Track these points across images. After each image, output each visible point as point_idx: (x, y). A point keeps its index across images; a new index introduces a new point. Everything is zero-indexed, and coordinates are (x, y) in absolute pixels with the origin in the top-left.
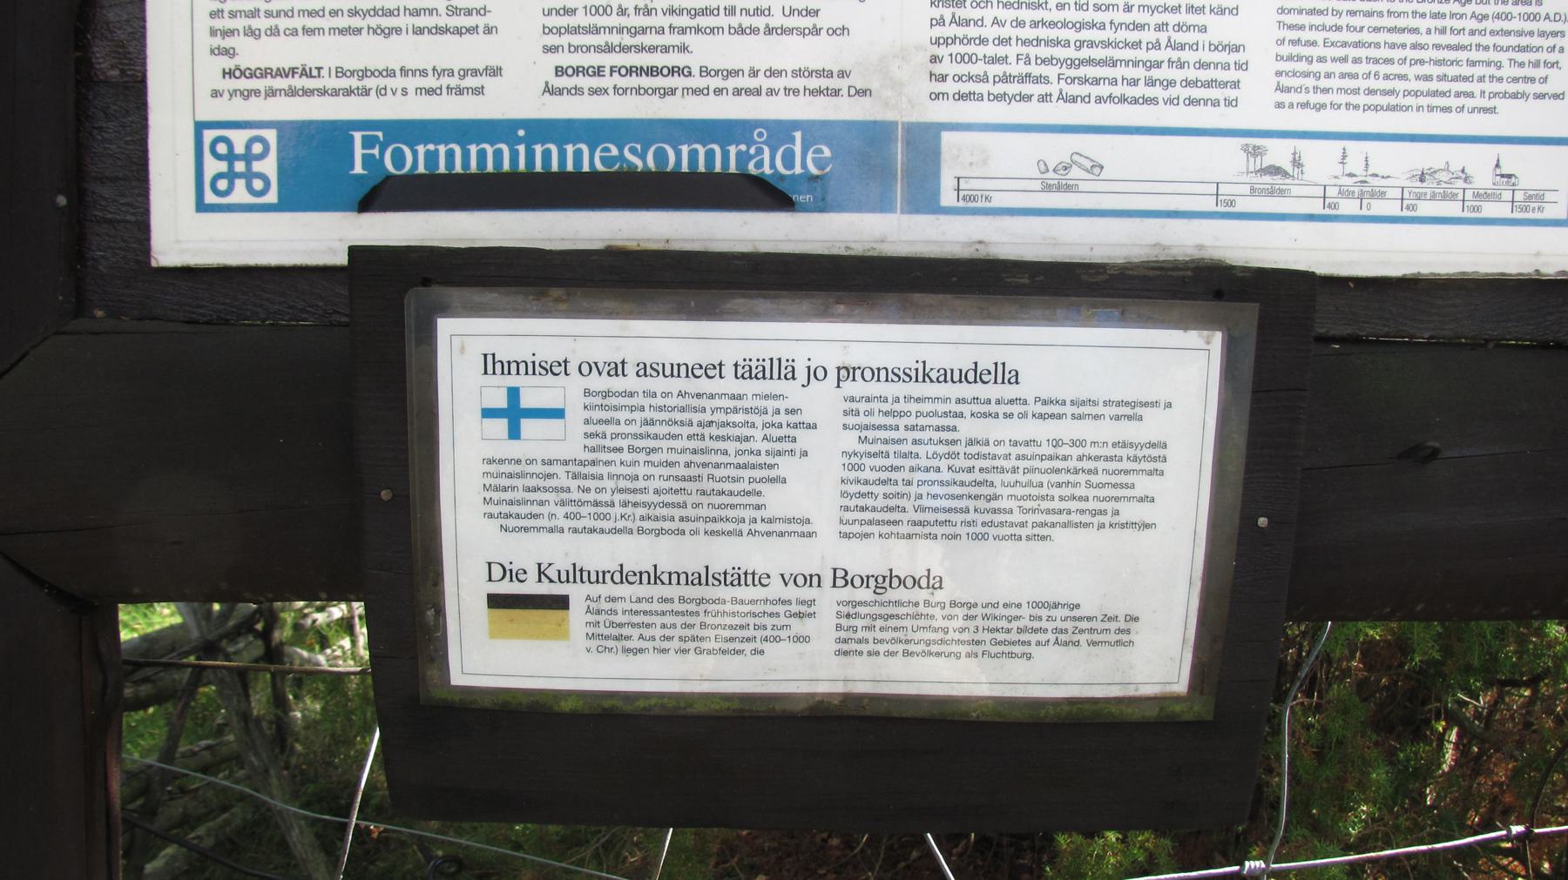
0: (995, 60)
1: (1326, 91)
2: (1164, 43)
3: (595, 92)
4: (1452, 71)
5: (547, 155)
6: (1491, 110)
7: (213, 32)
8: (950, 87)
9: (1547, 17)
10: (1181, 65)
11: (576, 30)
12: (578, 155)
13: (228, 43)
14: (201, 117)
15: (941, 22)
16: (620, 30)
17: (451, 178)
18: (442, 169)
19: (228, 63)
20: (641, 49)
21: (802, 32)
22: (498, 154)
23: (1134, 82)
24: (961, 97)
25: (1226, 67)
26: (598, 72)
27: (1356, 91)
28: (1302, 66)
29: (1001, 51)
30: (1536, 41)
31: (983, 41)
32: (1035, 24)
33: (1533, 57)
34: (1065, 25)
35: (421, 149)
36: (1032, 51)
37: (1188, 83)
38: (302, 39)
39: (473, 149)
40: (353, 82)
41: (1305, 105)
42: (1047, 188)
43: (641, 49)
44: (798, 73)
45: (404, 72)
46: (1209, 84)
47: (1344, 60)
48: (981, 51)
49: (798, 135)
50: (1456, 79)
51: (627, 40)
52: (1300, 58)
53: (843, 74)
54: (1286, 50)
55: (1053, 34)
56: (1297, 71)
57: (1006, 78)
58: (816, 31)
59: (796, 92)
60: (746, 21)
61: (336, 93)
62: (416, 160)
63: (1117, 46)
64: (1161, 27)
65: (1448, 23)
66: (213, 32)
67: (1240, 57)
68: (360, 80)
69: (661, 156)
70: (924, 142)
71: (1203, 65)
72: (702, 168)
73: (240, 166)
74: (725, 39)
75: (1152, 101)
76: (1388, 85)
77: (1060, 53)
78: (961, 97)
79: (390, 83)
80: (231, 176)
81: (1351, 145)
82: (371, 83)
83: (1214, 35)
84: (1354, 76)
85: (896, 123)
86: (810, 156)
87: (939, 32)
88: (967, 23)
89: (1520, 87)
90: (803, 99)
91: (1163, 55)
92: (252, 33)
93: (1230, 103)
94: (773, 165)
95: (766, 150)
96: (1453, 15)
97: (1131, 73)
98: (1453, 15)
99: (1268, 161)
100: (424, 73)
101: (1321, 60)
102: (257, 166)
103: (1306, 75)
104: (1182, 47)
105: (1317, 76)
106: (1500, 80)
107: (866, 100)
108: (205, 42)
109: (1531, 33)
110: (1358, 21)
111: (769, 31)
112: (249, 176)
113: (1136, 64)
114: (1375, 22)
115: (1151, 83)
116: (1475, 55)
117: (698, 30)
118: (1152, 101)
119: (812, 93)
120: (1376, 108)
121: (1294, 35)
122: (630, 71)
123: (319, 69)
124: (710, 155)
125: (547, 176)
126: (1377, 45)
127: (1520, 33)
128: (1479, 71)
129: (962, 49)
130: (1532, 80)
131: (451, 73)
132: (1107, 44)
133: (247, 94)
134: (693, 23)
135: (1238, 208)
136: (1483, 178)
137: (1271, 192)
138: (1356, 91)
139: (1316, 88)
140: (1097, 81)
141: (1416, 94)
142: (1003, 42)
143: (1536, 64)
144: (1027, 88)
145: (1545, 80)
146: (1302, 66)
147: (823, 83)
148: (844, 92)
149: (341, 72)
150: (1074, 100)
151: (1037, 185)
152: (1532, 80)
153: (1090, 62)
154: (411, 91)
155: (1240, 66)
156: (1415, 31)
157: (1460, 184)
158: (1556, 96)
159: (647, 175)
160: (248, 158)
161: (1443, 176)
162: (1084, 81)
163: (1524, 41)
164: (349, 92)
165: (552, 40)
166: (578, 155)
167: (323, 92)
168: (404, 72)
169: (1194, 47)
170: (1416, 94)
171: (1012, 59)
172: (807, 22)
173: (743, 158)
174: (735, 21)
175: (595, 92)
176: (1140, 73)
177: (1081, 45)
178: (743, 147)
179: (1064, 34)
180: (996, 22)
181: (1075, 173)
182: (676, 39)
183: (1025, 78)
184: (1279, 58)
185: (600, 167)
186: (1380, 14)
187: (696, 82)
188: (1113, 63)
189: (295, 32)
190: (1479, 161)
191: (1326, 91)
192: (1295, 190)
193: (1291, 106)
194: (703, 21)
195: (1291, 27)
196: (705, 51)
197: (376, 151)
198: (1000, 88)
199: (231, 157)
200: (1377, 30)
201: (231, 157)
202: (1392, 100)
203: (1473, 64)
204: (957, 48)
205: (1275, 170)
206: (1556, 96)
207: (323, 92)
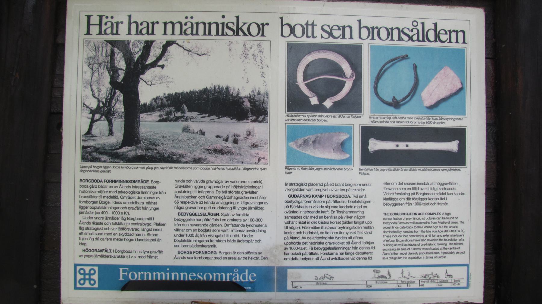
0: (303, 249)
1: (397, 254)
2: (351, 242)
3: (189, 258)
4: (433, 247)
5: (175, 276)
6: (444, 257)
7: (80, 239)
8: (290, 256)
9: (459, 231)
10: (356, 248)
11: (184, 241)
12: (184, 276)
13: (84, 242)
14: (76, 262)
15: (287, 238)
16: (196, 241)
17: (148, 282)
18: (145, 279)
19: (84, 248)
20: (202, 246)
21: (248, 242)
22: (161, 275)
23: (342, 254)
24: (293, 259)
25: (369, 248)
26: (190, 252)
27: (406, 254)
28: (390, 247)
29: (304, 246)
30: (456, 238)
31: (299, 243)
32: (314, 238)
33: (455, 242)
34: (323, 238)
35: (139, 273)
36: (313, 246)
37: (358, 253)
38: (105, 241)
39: (154, 274)
40: (120, 254)
41: (391, 258)
42: (318, 284)
43: (202, 246)
44: (247, 253)
45: (135, 251)
46: (364, 253)
47: (402, 245)
48: (299, 246)
49: (247, 270)
50: (434, 249)
51: (198, 244)
52: (390, 245)
53: (259, 253)
54: (385, 243)
55: (319, 241)
56: (389, 249)
57: (306, 254)
58: (252, 241)
59: (246, 258)
60: (232, 239)
61: (115, 257)
62: (138, 276)
63: (337, 244)
64: (350, 238)
65: (432, 233)
66: (80, 239)
67: (373, 245)
68: (122, 253)
69: (208, 276)
70: (283, 272)
71: (362, 248)
72: (219, 280)
73: (87, 277)
74: (226, 244)
75: (348, 259)
76: (415, 251)
77: (321, 246)
78: (293, 259)
79: (130, 254)
80: (85, 279)
81: (405, 269)
82: (125, 254)
83: (365, 240)
84: (405, 249)
85: (274, 267)
86: (250, 276)
87: (287, 241)
88: (295, 238)
89: (452, 250)
90: (248, 261)
91: (351, 246)
92: (91, 239)
93: (370, 258)
94: (239, 279)
95: (238, 275)
96: (433, 231)
97: (341, 251)
98: (433, 231)
99: (381, 274)
100: (140, 252)
101: (396, 245)
102: (92, 277)
103: (391, 250)
104: (356, 243)
105: (395, 250)
106: (446, 249)
107: (266, 261)
108: (77, 241)
109: (455, 236)
110: (406, 234)
111: (239, 241)
112: (90, 279)
113: (343, 248)
114: (411, 234)
115: (347, 254)
116: (439, 242)
117: (218, 241)
118: (348, 259)
119: (251, 259)
120: (412, 258)
121: (388, 239)
122: (199, 252)
123: (110, 250)
124: (222, 276)
125: (175, 281)
126: (412, 241)
127: (451, 236)
128: (440, 246)
129: (293, 246)
130: (456, 248)
131: (148, 252)
132: (334, 243)
133: (90, 256)
134: (217, 239)
135: (372, 288)
136: (443, 276)
137: (382, 283)
138: (406, 254)
139: (394, 253)
140: (332, 254)
141: (423, 254)
142: (305, 243)
143: (456, 244)
144: (312, 256)
145: (459, 248)
146: (390, 247)
147: (254, 256)
148: (260, 258)
149: (116, 251)
150: (325, 259)
151: (315, 283)
152: (456, 248)
153: (329, 248)
154: (137, 257)
155: (372, 248)
156: (422, 236)
157: (436, 278)
158: (462, 253)
159: (204, 282)
160: (90, 274)
161: (431, 276)
162: (328, 254)
163: (453, 238)
164: (119, 257)
165: (177, 243)
166: (184, 276)
167: (112, 257)
168: (135, 251)
169: (359, 243)
170: (423, 254)
171: (308, 248)
172: (249, 239)
173: (231, 277)
174: (229, 239)
175: (189, 258)
176: (344, 251)
177: (327, 244)
178: (231, 274)
179: (322, 241)
180: (303, 238)
181: (326, 279)
182: (212, 244)
183: (311, 253)
184: (384, 245)
185: (190, 279)
186: (412, 232)
187: (218, 256)
188: (336, 249)
189: (103, 240)
190: (441, 272)
191: (397, 254)
192: (389, 282)
193: (387, 258)
194: (220, 239)
195: (387, 237)
196: (221, 247)
197: (126, 274)
198: (304, 256)
199: (84, 274)
200: (411, 236)
201: (84, 274)
202: (416, 256)
203: (439, 244)
204: (292, 246)
205: (383, 277)
206: (462, 253)
207: (112, 257)
